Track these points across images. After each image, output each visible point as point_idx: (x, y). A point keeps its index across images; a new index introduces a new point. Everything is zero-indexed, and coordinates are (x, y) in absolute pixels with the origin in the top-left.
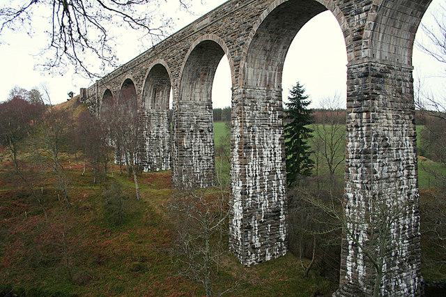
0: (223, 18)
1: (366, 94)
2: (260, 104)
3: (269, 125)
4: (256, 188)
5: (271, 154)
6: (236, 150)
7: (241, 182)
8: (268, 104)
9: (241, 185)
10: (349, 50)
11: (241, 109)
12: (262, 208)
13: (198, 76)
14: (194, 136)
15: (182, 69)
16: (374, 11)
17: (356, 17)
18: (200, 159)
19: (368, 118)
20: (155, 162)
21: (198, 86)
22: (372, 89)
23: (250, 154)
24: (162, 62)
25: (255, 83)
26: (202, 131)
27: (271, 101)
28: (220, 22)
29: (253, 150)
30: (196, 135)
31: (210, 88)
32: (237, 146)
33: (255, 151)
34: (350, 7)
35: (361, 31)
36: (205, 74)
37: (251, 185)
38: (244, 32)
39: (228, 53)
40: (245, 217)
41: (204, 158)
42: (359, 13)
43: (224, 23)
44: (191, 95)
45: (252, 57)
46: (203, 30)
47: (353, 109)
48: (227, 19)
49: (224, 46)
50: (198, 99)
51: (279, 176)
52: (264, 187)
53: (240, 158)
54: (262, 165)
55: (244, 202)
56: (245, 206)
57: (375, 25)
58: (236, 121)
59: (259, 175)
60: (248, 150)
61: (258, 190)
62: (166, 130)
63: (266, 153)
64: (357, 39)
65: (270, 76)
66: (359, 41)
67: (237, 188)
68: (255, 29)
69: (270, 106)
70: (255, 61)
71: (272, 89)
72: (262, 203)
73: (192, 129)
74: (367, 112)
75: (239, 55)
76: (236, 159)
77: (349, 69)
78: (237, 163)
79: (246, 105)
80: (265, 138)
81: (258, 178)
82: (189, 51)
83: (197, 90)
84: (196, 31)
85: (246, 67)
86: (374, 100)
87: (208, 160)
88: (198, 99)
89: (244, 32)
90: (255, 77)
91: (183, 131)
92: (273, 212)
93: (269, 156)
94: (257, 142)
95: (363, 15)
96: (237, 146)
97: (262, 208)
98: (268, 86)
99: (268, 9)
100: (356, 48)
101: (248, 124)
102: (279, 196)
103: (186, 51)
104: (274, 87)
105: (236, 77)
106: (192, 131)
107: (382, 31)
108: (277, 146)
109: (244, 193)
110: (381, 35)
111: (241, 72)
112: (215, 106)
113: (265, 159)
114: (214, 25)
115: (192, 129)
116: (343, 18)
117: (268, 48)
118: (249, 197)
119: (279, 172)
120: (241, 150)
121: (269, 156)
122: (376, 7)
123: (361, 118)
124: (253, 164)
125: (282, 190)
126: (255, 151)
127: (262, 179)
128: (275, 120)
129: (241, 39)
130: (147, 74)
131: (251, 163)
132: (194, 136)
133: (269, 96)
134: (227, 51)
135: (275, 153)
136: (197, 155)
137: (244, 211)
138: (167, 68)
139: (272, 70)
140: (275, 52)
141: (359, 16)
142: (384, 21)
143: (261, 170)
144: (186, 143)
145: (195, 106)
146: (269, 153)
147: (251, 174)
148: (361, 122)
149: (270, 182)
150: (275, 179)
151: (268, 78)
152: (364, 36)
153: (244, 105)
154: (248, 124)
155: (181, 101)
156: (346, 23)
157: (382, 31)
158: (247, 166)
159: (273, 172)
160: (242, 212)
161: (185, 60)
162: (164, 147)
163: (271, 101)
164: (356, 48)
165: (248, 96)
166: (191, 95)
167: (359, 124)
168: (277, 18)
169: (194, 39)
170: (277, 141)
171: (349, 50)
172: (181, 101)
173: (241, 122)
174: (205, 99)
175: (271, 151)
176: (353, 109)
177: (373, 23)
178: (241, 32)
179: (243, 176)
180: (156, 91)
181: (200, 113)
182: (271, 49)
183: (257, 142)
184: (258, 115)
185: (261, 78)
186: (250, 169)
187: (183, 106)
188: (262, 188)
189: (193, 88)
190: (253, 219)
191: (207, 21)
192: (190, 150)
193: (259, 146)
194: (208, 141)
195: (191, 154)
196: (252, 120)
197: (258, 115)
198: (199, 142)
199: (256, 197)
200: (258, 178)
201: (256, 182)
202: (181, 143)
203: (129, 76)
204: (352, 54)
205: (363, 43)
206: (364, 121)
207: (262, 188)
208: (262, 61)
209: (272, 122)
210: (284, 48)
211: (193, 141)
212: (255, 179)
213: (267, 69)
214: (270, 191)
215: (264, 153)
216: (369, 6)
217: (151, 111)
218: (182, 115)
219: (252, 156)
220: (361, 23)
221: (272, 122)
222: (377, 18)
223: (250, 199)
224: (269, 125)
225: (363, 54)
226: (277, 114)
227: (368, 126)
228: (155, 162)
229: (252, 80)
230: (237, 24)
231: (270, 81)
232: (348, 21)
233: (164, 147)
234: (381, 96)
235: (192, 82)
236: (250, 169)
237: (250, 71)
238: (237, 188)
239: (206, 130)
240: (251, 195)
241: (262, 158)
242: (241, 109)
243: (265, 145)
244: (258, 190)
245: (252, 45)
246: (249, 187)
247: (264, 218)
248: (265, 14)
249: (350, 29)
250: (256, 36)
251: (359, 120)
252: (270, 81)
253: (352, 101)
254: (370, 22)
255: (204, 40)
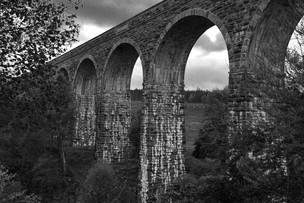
0: (138, 26)
1: (242, 96)
2: (165, 97)
3: (173, 115)
4: (160, 166)
5: (173, 138)
6: (145, 134)
7: (147, 160)
8: (172, 98)
9: (148, 163)
10: (231, 60)
11: (149, 101)
12: (165, 183)
13: (119, 70)
14: (114, 120)
15: (106, 65)
16: (250, 31)
17: (237, 34)
18: (119, 138)
19: (244, 116)
20: (83, 138)
21: (119, 78)
22: (248, 93)
23: (156, 138)
24: (90, 57)
25: (161, 81)
26: (121, 115)
27: (175, 95)
28: (135, 29)
29: (158, 134)
30: (116, 118)
31: (129, 80)
32: (145, 131)
33: (160, 135)
34: (232, 27)
35: (240, 45)
36: (125, 69)
37: (156, 163)
38: (153, 39)
39: (141, 55)
40: (150, 190)
41: (122, 137)
42: (239, 31)
43: (138, 31)
44: (113, 86)
45: (159, 59)
46: (123, 34)
47: (233, 108)
48: (141, 27)
49: (138, 49)
50: (118, 89)
51: (180, 156)
52: (167, 165)
53: (147, 141)
54: (165, 147)
55: (149, 177)
56: (151, 181)
57: (251, 41)
58: (145, 111)
59: (163, 155)
60: (154, 135)
61: (162, 167)
62: (93, 112)
63: (169, 137)
64: (237, 52)
65: (175, 74)
66: (238, 54)
67: (145, 165)
68: (162, 37)
69: (173, 99)
70: (161, 63)
71: (175, 85)
72: (165, 179)
73: (113, 113)
74: (243, 111)
75: (149, 57)
76: (144, 141)
77: (230, 75)
78: (145, 144)
79: (154, 98)
80: (169, 125)
81: (162, 157)
82: (112, 51)
83: (118, 82)
84: (117, 34)
85: (154, 67)
86: (249, 101)
87: (125, 139)
88: (118, 89)
89: (153, 39)
90: (161, 76)
91: (106, 116)
92: (174, 186)
93: (172, 139)
94: (162, 128)
95: (242, 33)
96: (145, 131)
97: (165, 183)
98: (172, 82)
99: (172, 22)
100: (236, 59)
101: (155, 114)
102: (179, 173)
103: (109, 50)
104: (177, 84)
105: (146, 75)
106: (112, 115)
107: (257, 46)
108: (179, 131)
109: (150, 170)
110: (256, 49)
111: (150, 71)
112: (186, 89)
113: (169, 142)
114: (131, 31)
115: (113, 113)
116: (227, 34)
117: (173, 52)
118: (154, 173)
119: (179, 152)
120: (148, 135)
121: (172, 139)
122: (252, 28)
123: (239, 116)
124: (158, 147)
125: (183, 168)
126: (160, 135)
127: (165, 159)
128: (178, 110)
129: (151, 44)
130: (79, 65)
131: (156, 145)
132: (114, 120)
133: (172, 91)
134: (141, 54)
135: (177, 138)
136: (117, 135)
137: (150, 185)
138: (94, 62)
139: (176, 70)
140: (179, 55)
141: (239, 33)
142: (259, 37)
143: (165, 151)
144: (107, 125)
145: (116, 95)
146: (172, 137)
147: (156, 154)
148: (239, 118)
149: (172, 161)
150: (177, 158)
151: (172, 77)
152: (242, 50)
153: (152, 98)
154: (155, 114)
155: (104, 91)
156: (229, 38)
157: (257, 46)
158: (153, 148)
159: (175, 153)
160: (148, 185)
161: (109, 57)
162: (91, 127)
163: (175, 95)
164: (236, 59)
165: (155, 90)
166: (113, 86)
167: (237, 121)
168: (179, 29)
169: (116, 41)
170: (179, 127)
171: (231, 60)
172: (104, 91)
173: (149, 112)
174: (124, 89)
175: (173, 135)
176: (233, 108)
177: (249, 40)
178: (151, 39)
179: (149, 157)
180: (86, 80)
181: (120, 101)
182: (175, 53)
183: (162, 128)
184: (163, 106)
185: (167, 76)
186: (156, 150)
187: (106, 95)
188: (166, 166)
189: (115, 80)
190: (157, 192)
191: (126, 27)
192: (111, 130)
193: (164, 131)
194: (126, 124)
195: (111, 134)
196: (158, 110)
197: (163, 106)
198: (118, 124)
199: (160, 173)
200: (162, 157)
201: (160, 161)
202: (103, 125)
203: (64, 66)
204: (234, 64)
205: (242, 56)
206: (241, 118)
207: (166, 166)
208: (168, 63)
209: (175, 112)
210: (186, 52)
211: (113, 124)
212: (160, 158)
213: (171, 69)
214: (171, 168)
215: (168, 137)
216: (246, 26)
217: (82, 96)
218: (105, 102)
219: (157, 140)
220: (240, 39)
221: (175, 112)
222: (252, 36)
223: (155, 175)
224: (173, 115)
225: (241, 64)
226: (180, 106)
227: (243, 122)
228: (83, 138)
229: (159, 78)
230: (148, 32)
231: (174, 78)
232: (231, 37)
233: (91, 127)
234: (256, 98)
235: (114, 75)
236: (156, 150)
237: (157, 71)
238: (144, 166)
239: (124, 115)
240: (156, 172)
241: (166, 141)
242: (149, 101)
243: (169, 130)
244: (162, 167)
245: (160, 50)
246: (154, 165)
247: (167, 191)
248: (169, 26)
249: (232, 44)
250: (163, 43)
251: (237, 117)
252: (174, 78)
253: (232, 101)
254: (247, 39)
255: (123, 42)
